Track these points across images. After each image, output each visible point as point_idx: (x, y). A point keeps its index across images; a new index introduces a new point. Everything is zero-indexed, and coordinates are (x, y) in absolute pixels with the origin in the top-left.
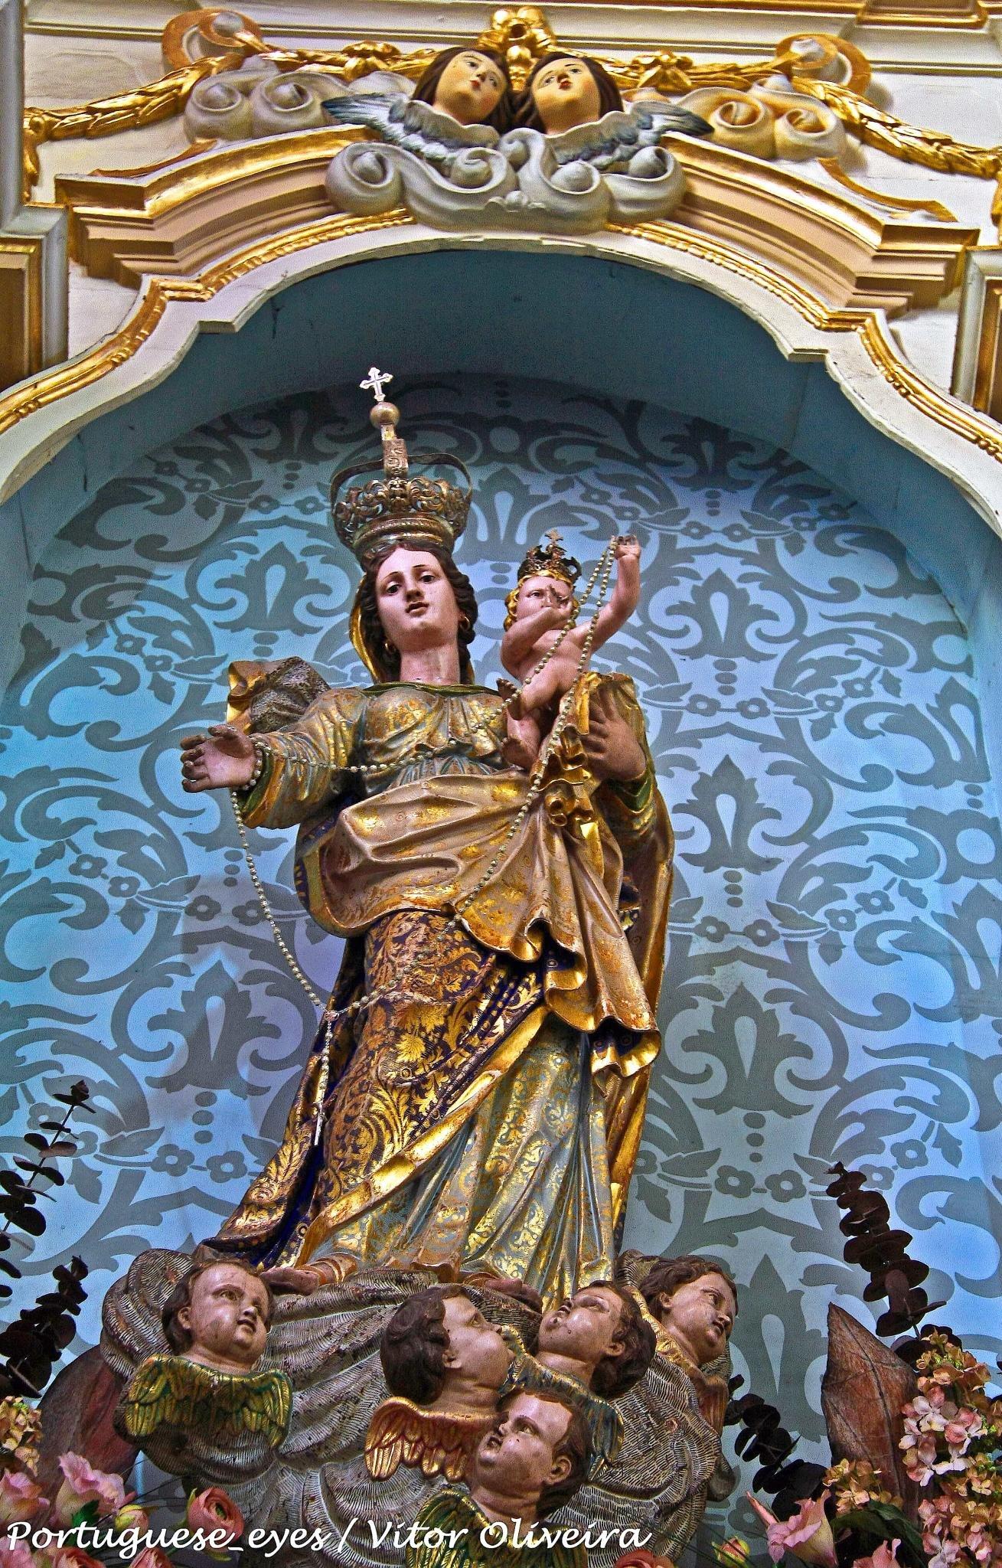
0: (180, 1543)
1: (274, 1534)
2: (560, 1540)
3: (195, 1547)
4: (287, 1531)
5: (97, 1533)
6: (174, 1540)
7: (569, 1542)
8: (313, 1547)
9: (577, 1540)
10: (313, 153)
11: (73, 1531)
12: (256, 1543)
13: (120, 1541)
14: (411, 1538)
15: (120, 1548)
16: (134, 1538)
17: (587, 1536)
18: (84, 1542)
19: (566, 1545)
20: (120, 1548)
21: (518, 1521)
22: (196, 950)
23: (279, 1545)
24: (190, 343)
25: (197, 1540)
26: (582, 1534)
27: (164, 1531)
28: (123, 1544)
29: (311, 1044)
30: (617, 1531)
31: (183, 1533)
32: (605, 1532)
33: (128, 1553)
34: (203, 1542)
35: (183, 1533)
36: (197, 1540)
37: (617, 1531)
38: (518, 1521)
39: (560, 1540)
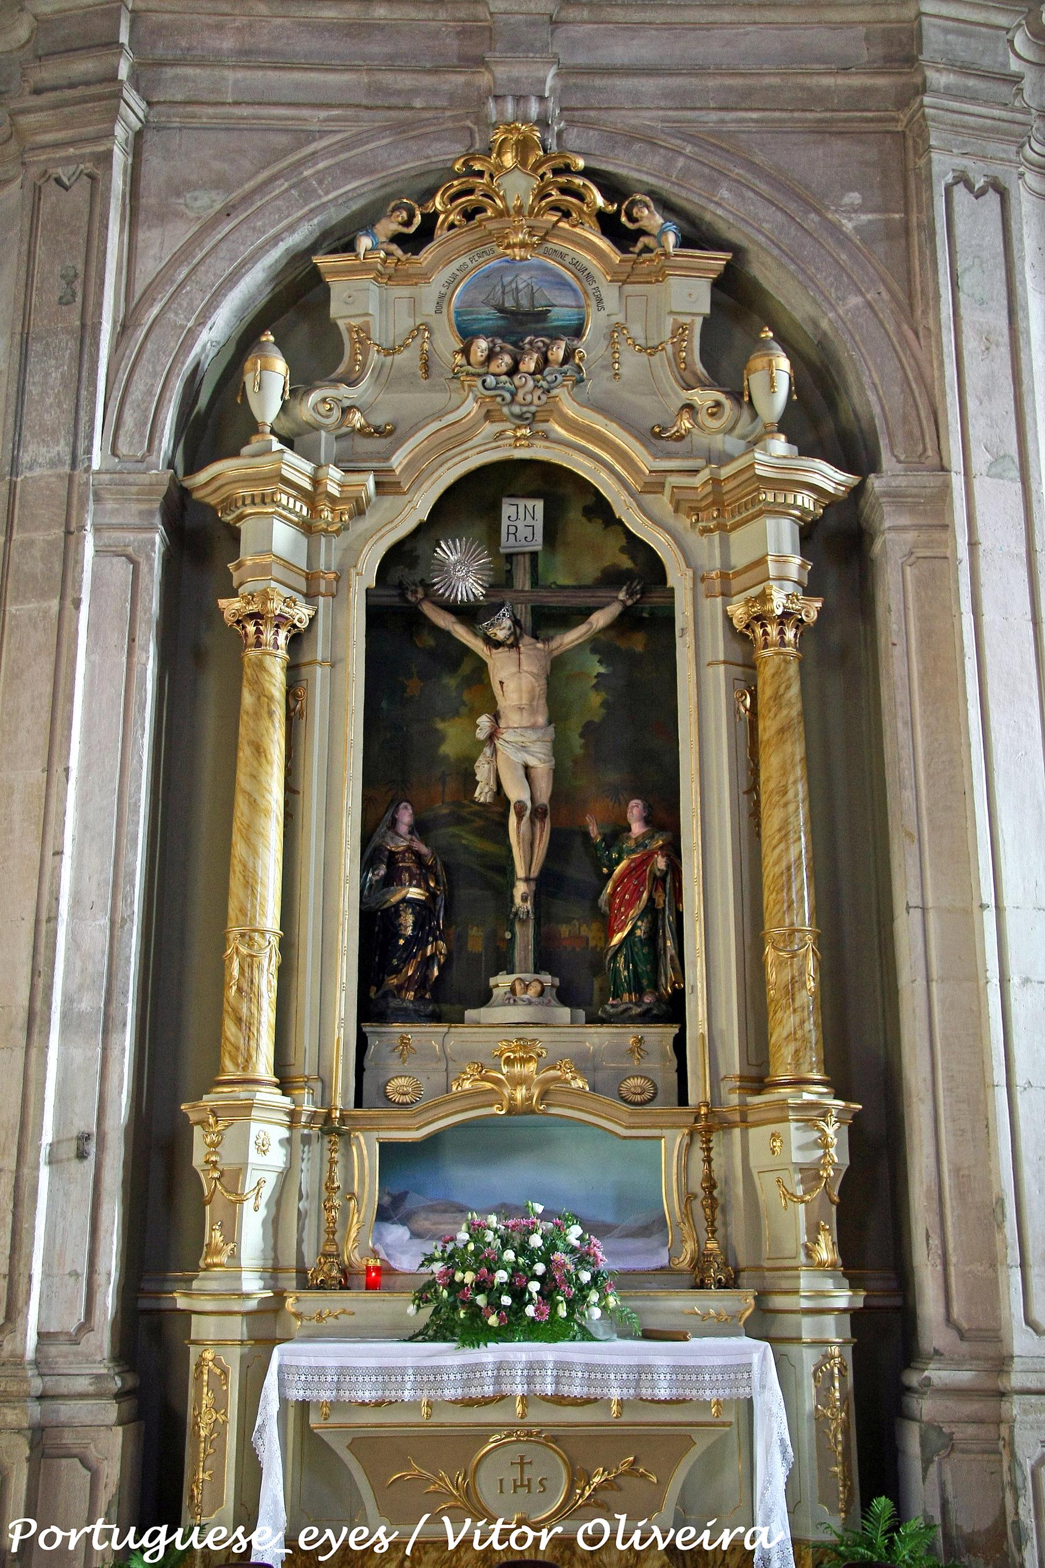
0: (216, 1543)
1: (329, 1533)
2: (346, 1540)
3: (235, 1549)
4: (345, 1530)
5: (116, 1532)
6: (209, 1541)
7: (685, 1544)
8: (376, 1549)
9: (223, 1541)
10: (578, 1039)
11: (88, 1529)
12: (308, 1544)
13: (145, 1541)
14: (494, 1538)
15: (142, 1550)
16: (161, 1537)
17: (706, 1535)
18: (100, 1543)
19: (680, 1547)
20: (142, 1550)
21: (623, 1518)
22: (418, 557)
23: (335, 1546)
24: (551, 783)
25: (237, 1541)
26: (699, 1534)
27: (133, 1529)
28: (147, 1545)
29: (472, 1490)
30: (741, 1529)
31: (219, 1532)
32: (727, 1531)
33: (153, 1556)
34: (244, 1543)
35: (219, 1532)
36: (237, 1541)
37: (741, 1529)
38: (623, 1518)
39: (346, 1540)
